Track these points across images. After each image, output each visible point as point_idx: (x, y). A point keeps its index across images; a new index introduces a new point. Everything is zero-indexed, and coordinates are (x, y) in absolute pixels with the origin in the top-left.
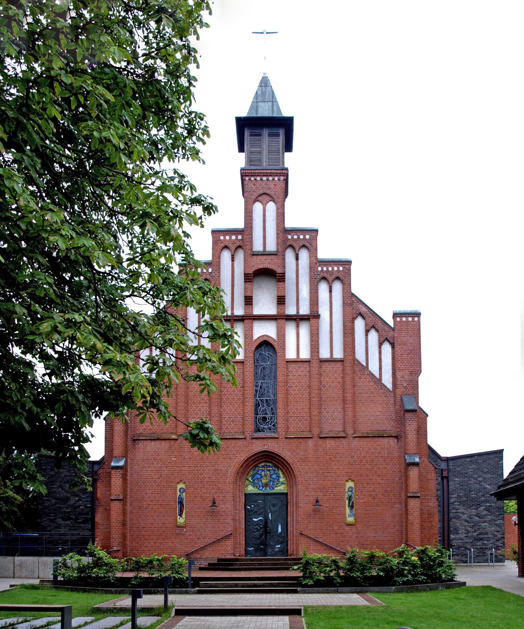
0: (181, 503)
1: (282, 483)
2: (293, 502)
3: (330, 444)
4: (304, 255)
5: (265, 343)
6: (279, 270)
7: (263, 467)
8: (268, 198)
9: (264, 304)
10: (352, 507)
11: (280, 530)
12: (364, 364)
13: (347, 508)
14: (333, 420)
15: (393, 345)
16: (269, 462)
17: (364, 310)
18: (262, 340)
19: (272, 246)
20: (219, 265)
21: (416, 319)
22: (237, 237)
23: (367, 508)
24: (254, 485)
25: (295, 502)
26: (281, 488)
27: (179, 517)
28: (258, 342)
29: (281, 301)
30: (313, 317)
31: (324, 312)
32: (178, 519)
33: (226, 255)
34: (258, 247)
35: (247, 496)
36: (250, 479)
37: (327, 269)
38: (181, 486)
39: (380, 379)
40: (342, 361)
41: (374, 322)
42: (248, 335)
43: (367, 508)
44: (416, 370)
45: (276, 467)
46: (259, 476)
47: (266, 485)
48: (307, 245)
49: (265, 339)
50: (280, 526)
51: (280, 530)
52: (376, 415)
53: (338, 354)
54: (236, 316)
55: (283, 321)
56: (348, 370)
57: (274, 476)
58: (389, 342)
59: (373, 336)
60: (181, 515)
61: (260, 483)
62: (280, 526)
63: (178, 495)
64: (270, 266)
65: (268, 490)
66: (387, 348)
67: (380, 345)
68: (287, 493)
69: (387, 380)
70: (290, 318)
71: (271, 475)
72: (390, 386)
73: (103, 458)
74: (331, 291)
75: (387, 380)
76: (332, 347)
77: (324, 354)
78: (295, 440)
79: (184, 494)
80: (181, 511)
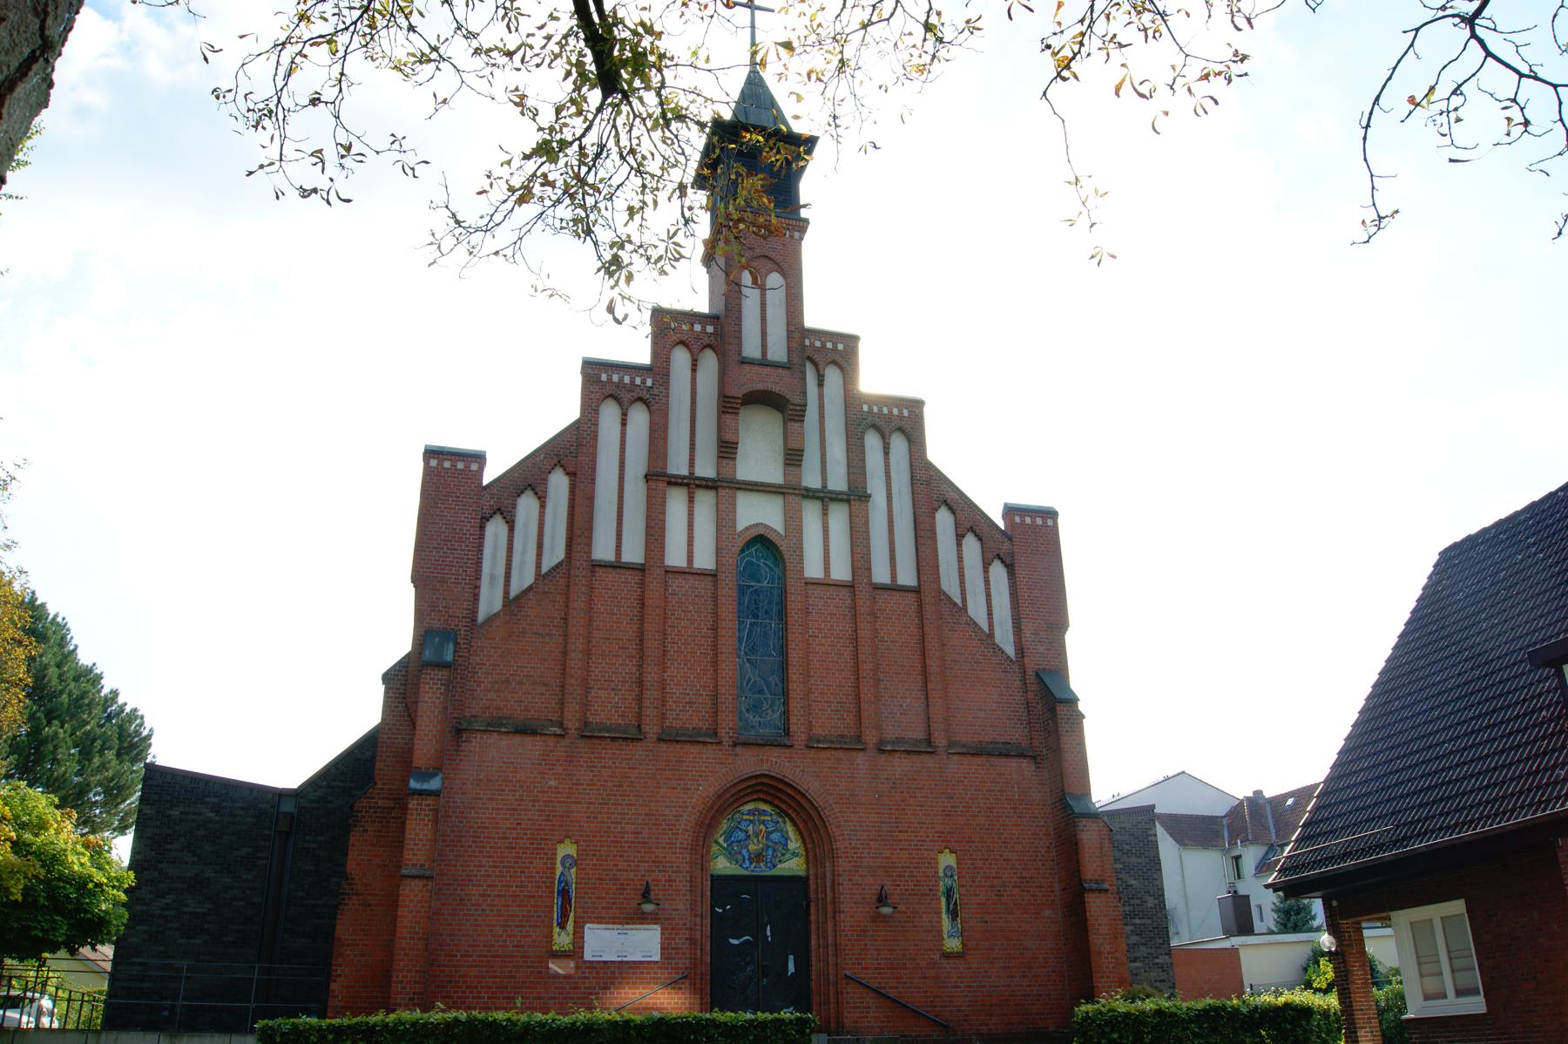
0: (564, 893)
1: (795, 854)
2: (825, 899)
3: (900, 766)
4: (833, 376)
5: (761, 541)
6: (795, 399)
7: (750, 813)
8: (770, 265)
9: (759, 457)
10: (954, 914)
11: (791, 968)
12: (959, 601)
13: (944, 916)
14: (900, 713)
15: (1011, 569)
16: (765, 801)
17: (951, 496)
18: (755, 532)
19: (778, 352)
20: (667, 375)
21: (474, 467)
22: (704, 328)
23: (987, 918)
24: (731, 856)
25: (829, 899)
26: (793, 865)
27: (557, 930)
28: (748, 536)
29: (793, 458)
30: (856, 496)
31: (876, 486)
32: (555, 936)
33: (681, 358)
34: (751, 349)
35: (719, 882)
36: (721, 840)
37: (644, 382)
38: (567, 849)
39: (991, 635)
40: (713, 575)
41: (969, 519)
42: (724, 521)
43: (987, 918)
44: (1056, 621)
45: (783, 813)
46: (742, 835)
47: (758, 857)
48: (840, 360)
49: (761, 531)
50: (791, 957)
51: (791, 968)
52: (986, 709)
53: (907, 577)
54: (831, 492)
55: (797, 499)
56: (929, 611)
57: (775, 836)
58: (1003, 562)
59: (971, 545)
60: (562, 926)
61: (744, 852)
62: (791, 957)
63: (558, 873)
64: (776, 389)
65: (763, 870)
66: (998, 572)
67: (986, 566)
68: (807, 877)
69: (1005, 638)
70: (809, 494)
71: (769, 833)
72: (1010, 651)
73: (354, 770)
74: (624, 424)
75: (1005, 638)
76: (894, 563)
77: (603, 550)
78: (828, 753)
79: (573, 871)
80: (564, 916)
